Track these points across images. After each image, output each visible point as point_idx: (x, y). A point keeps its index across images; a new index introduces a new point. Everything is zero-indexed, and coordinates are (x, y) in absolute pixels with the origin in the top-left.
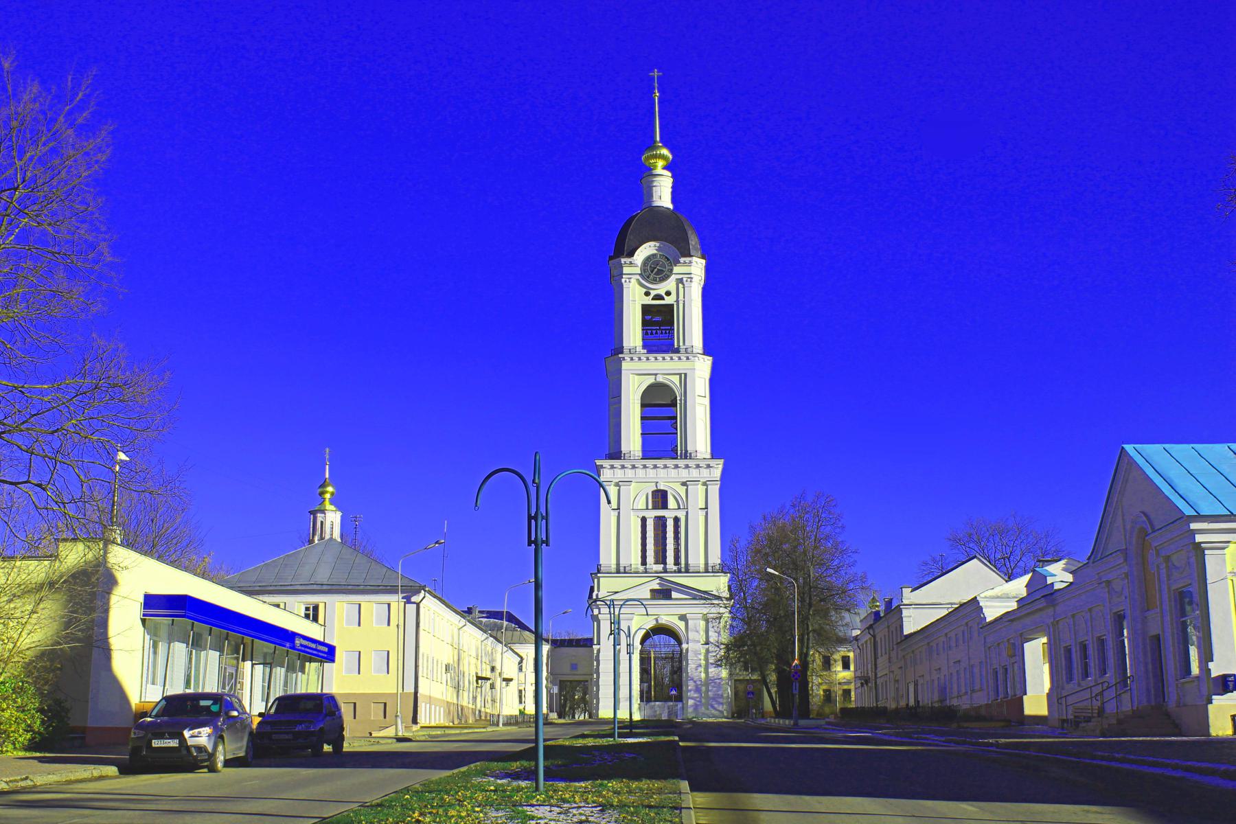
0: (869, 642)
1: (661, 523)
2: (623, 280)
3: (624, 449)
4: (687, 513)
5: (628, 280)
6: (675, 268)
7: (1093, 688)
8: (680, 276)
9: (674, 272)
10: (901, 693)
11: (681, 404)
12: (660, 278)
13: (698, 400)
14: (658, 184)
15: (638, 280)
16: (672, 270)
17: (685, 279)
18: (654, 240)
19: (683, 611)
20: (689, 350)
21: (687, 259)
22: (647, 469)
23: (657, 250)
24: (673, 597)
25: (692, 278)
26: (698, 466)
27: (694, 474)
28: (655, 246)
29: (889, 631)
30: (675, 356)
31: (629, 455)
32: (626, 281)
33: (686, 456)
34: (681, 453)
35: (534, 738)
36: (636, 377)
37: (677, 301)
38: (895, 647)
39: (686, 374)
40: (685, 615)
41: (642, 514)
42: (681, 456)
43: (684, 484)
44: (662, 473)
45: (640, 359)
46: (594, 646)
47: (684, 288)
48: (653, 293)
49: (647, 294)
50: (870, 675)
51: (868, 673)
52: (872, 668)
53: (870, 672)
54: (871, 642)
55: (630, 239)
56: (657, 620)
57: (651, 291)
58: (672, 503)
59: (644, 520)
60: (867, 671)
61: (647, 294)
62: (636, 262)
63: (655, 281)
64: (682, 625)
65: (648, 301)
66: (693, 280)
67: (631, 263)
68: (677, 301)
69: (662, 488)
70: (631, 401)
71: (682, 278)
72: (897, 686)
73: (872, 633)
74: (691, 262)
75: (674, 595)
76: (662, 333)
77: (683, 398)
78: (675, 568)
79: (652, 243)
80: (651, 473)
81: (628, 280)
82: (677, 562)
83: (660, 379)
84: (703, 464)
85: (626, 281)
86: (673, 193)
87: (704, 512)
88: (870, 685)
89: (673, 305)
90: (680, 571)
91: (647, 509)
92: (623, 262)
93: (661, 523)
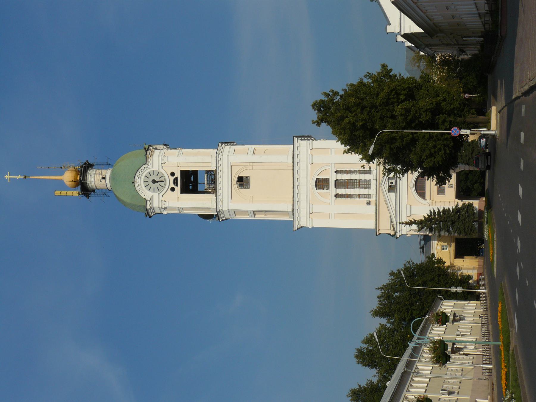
1: (338, 184)
48: (172, 185)
49: (173, 189)
59: (337, 196)
65: (178, 189)
93: (338, 184)
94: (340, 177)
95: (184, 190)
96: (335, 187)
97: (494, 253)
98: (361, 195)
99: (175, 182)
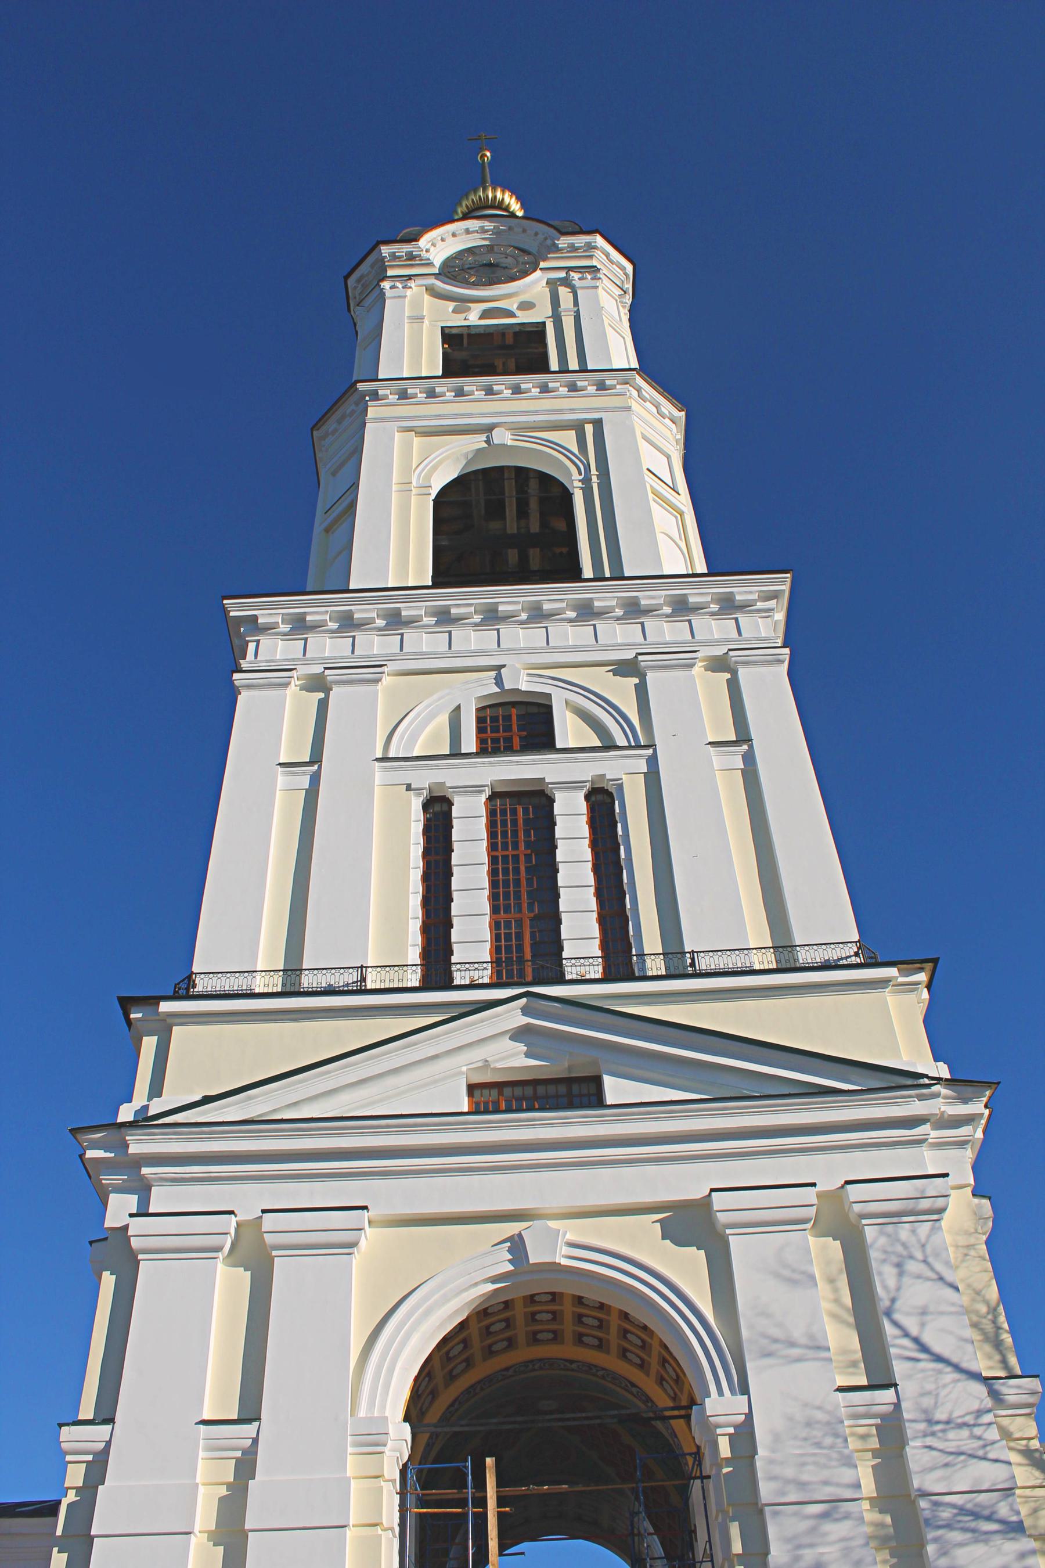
4: (653, 761)
7: (710, 1564)
36: (417, 441)
39: (598, 424)
40: (705, 1203)
41: (426, 778)
43: (625, 668)
44: (517, 636)
45: (431, 394)
56: (517, 1246)
75: (615, 1088)
89: (544, 323)
91: (456, 754)
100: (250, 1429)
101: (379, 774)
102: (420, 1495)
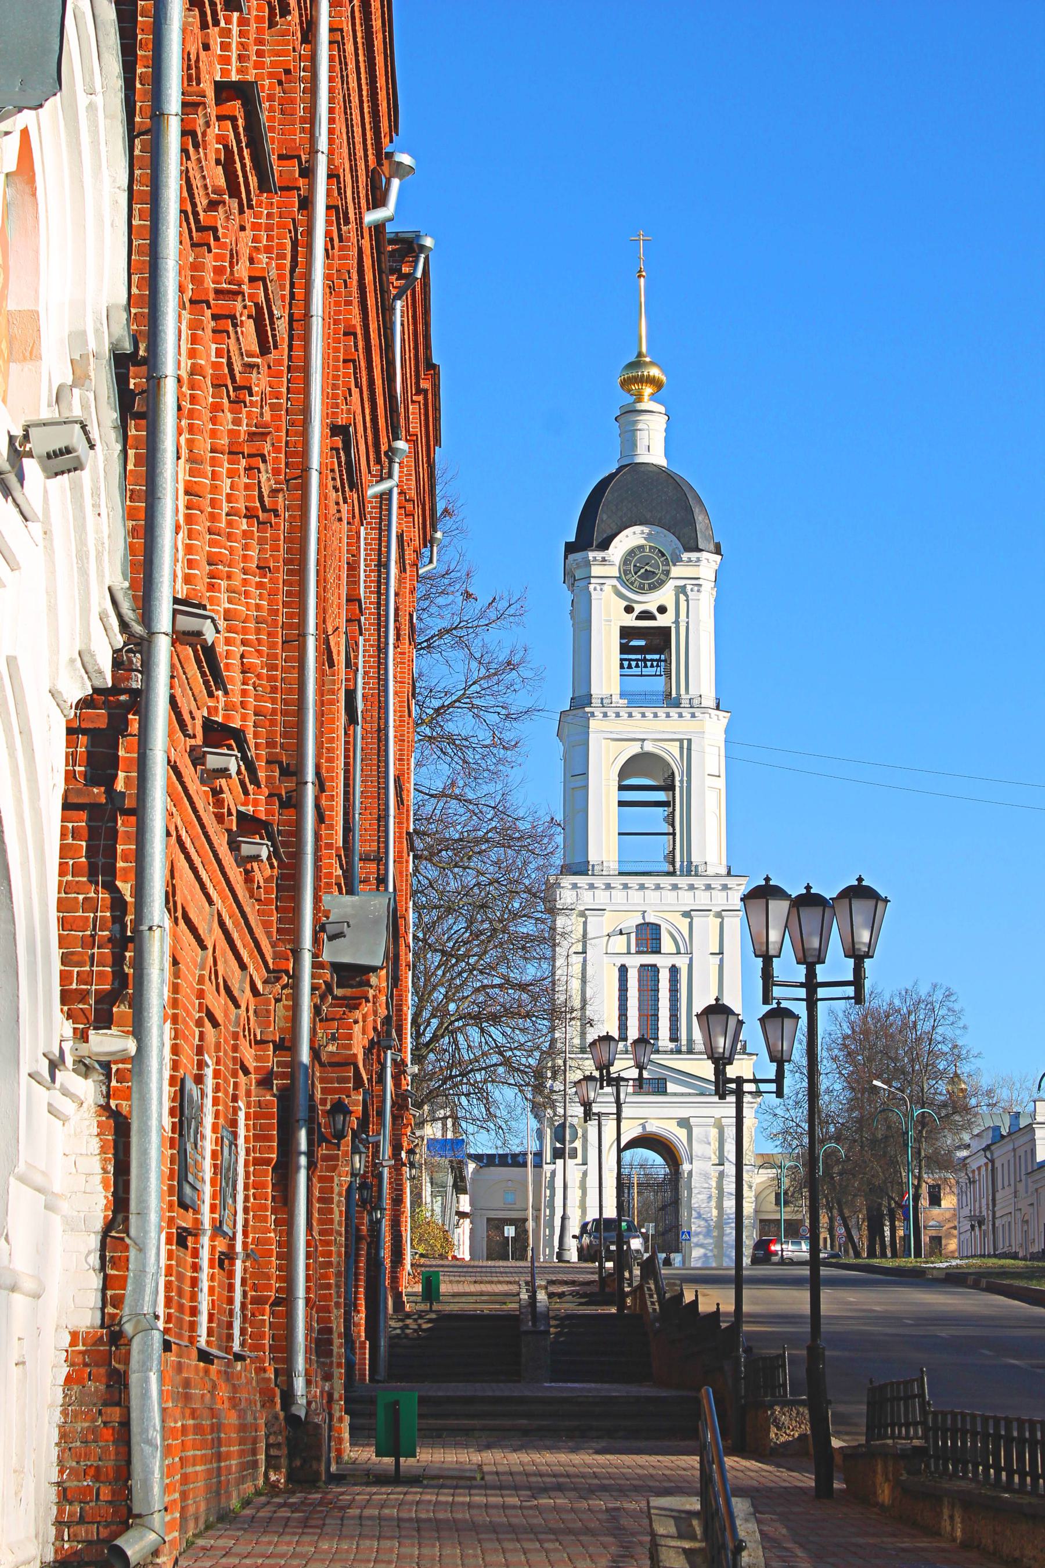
0: (983, 1169)
1: (649, 972)
2: (591, 587)
3: (593, 858)
4: (691, 959)
5: (598, 588)
6: (673, 568)
8: (681, 583)
9: (672, 575)
10: (1031, 1237)
11: (681, 788)
12: (636, 555)
13: (710, 781)
14: (645, 427)
15: (614, 586)
16: (667, 573)
17: (689, 588)
18: (641, 524)
19: (683, 1113)
20: (696, 702)
21: (694, 556)
22: (629, 891)
23: (645, 539)
24: (669, 1091)
25: (700, 585)
26: (708, 887)
27: (702, 899)
28: (643, 533)
29: (1015, 1156)
30: (674, 712)
31: (600, 868)
32: (595, 589)
33: (690, 870)
34: (682, 865)
35: (733, 1272)
37: (677, 622)
38: (1023, 1177)
39: (689, 741)
42: (681, 871)
43: (687, 914)
44: (652, 896)
45: (618, 715)
46: (545, 1166)
47: (687, 601)
48: (638, 608)
49: (629, 610)
50: (984, 1213)
51: (981, 1212)
52: (988, 1204)
53: (984, 1209)
54: (987, 1170)
55: (602, 520)
56: (644, 1127)
57: (635, 605)
58: (667, 944)
59: (623, 970)
60: (980, 1208)
61: (629, 610)
62: (612, 558)
63: (641, 590)
64: (682, 1134)
65: (630, 621)
66: (702, 589)
67: (604, 560)
68: (677, 622)
69: (652, 921)
70: (604, 783)
71: (685, 586)
72: (1025, 1228)
73: (989, 1156)
74: (698, 560)
75: (671, 1087)
76: (646, 666)
77: (685, 778)
78: (672, 1046)
79: (638, 529)
80: (636, 896)
81: (598, 588)
82: (674, 1038)
83: (649, 747)
84: (716, 883)
85: (595, 589)
86: (667, 440)
87: (716, 959)
88: (983, 1227)
90: (679, 1052)
91: (629, 953)
92: (591, 558)
93: (649, 972)
94: (664, 976)
95: (626, 633)
96: (641, 966)
97: (578, 1265)
98: (549, 954)
99: (646, 615)
100: (585, 1167)
101: (606, 959)
102: (532, 972)
